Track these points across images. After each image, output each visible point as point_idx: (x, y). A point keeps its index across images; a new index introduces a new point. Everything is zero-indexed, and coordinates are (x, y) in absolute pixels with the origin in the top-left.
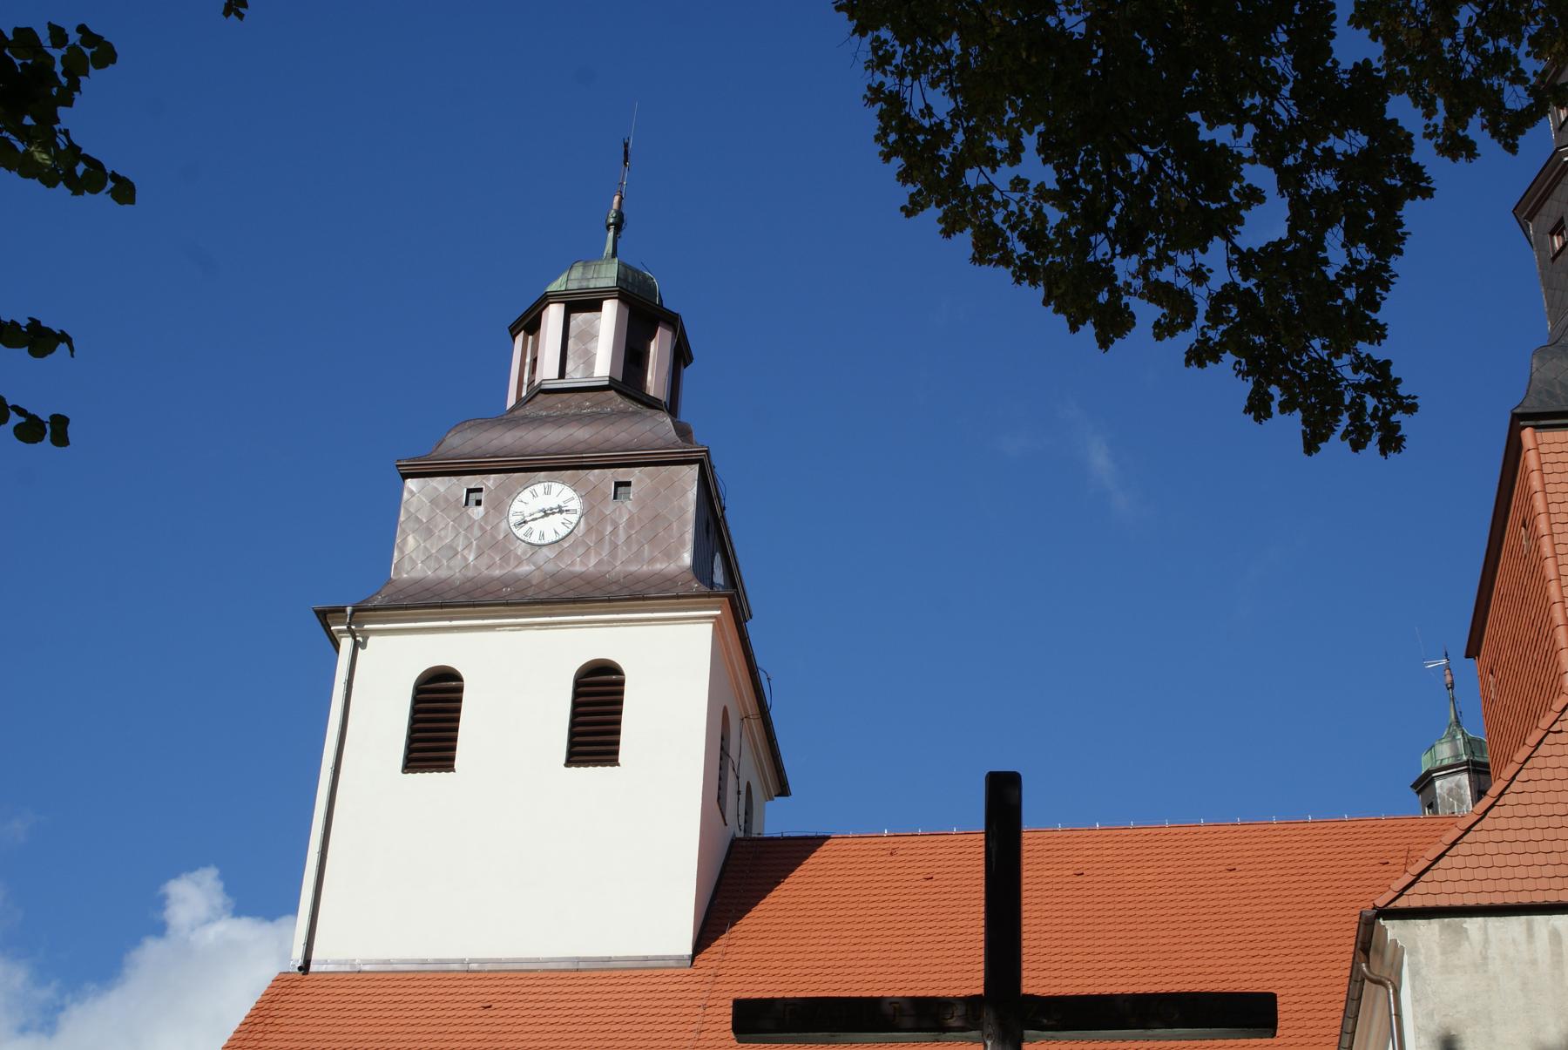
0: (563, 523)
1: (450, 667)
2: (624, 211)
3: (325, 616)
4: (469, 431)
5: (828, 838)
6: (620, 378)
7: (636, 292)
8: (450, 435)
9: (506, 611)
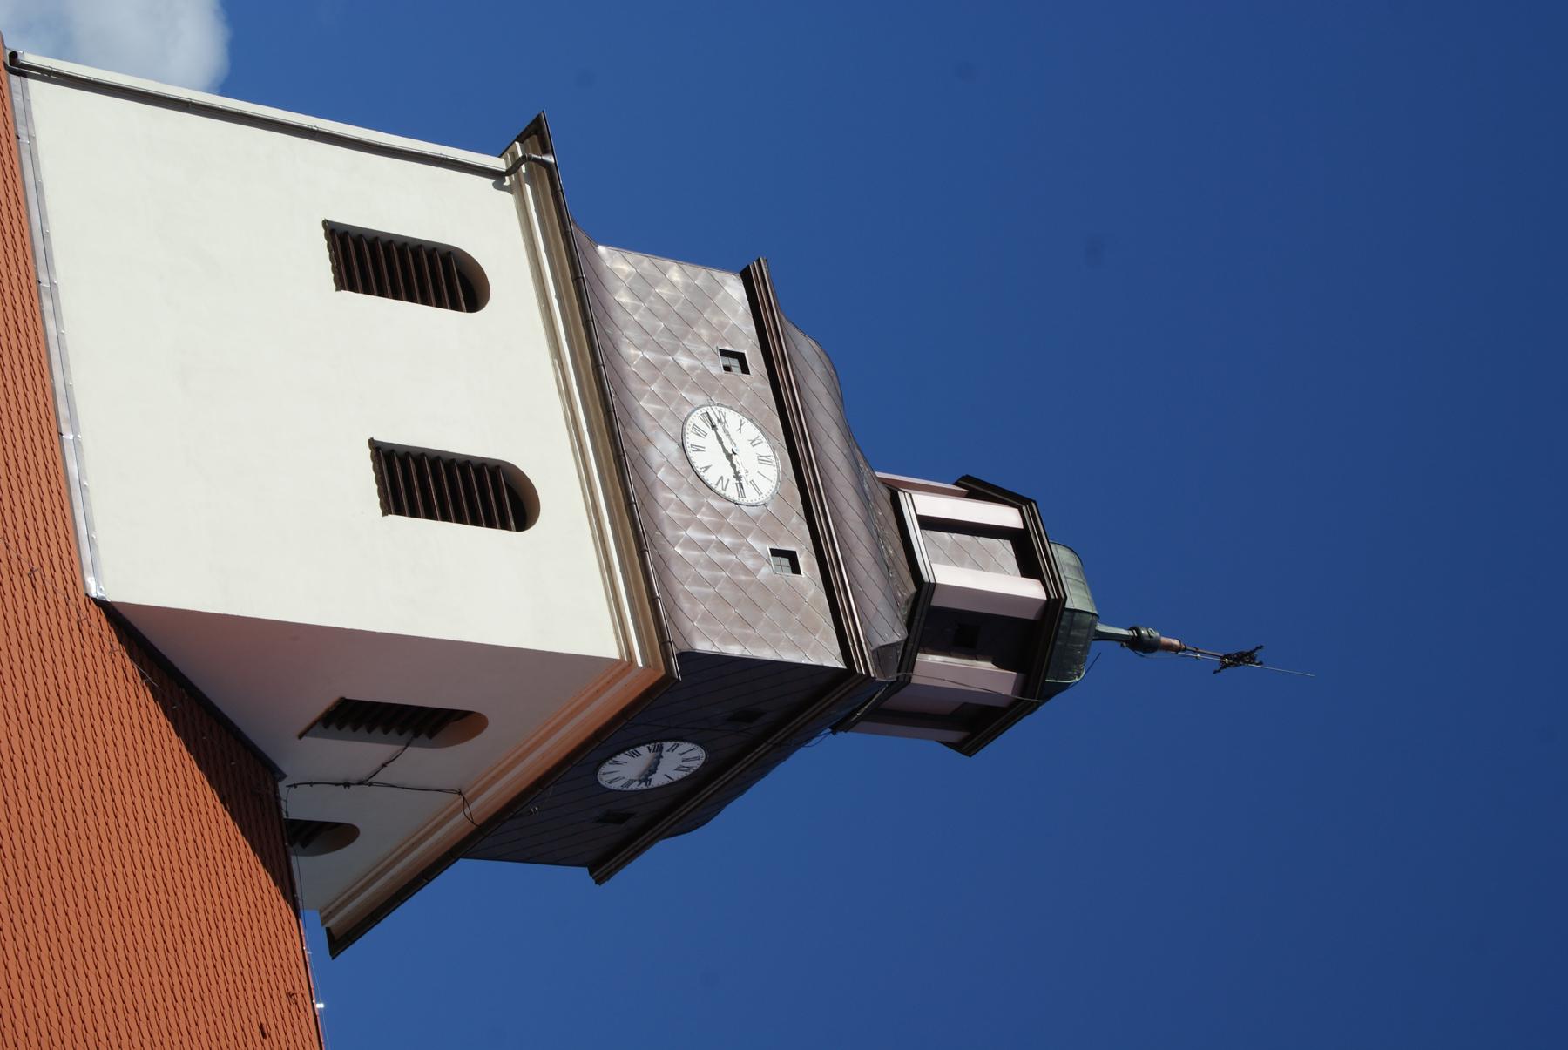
0: (722, 478)
1: (488, 300)
2: (1158, 654)
3: (536, 132)
4: (824, 370)
5: (298, 917)
6: (937, 601)
7: (1059, 643)
8: (813, 343)
9: (586, 368)
